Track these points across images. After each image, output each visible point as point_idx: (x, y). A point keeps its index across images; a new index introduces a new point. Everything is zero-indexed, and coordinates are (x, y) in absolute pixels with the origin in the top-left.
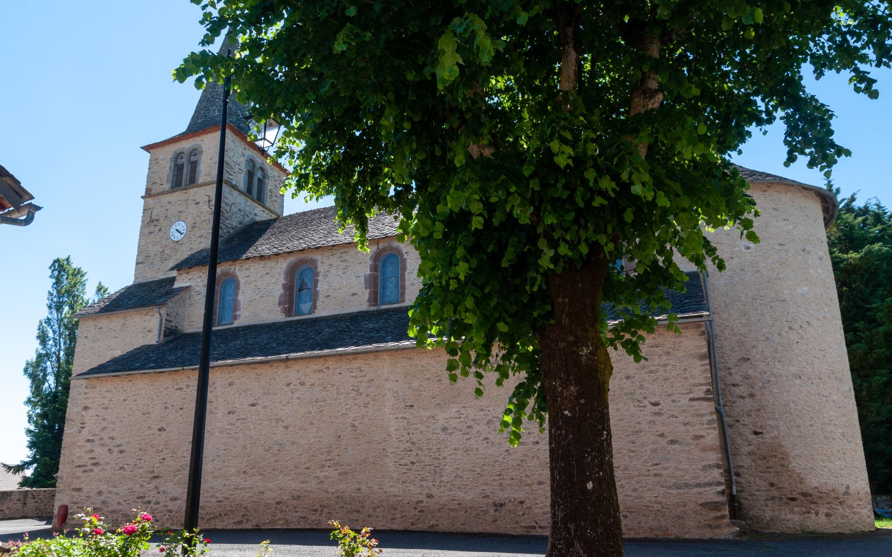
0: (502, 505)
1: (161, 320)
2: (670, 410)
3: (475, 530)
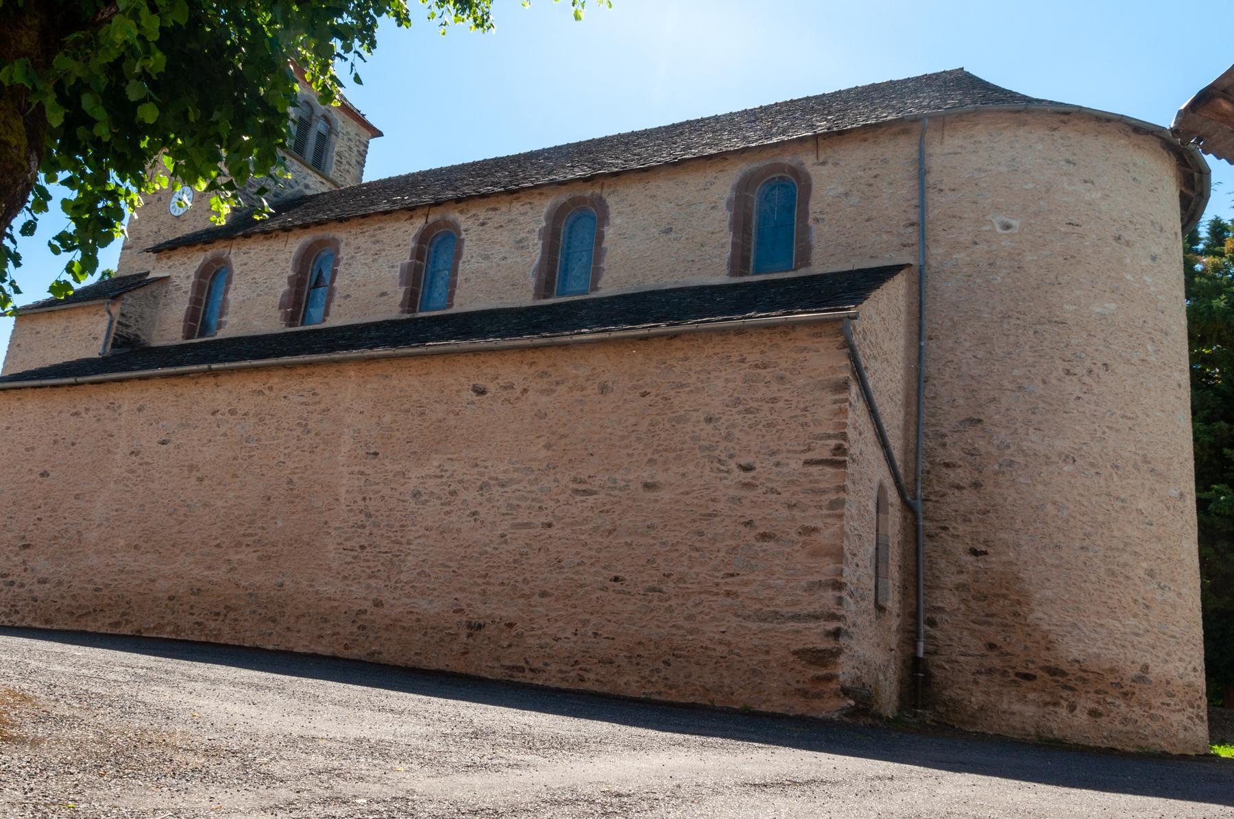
0: (480, 627)
1: (111, 322)
2: (769, 479)
3: (434, 666)
